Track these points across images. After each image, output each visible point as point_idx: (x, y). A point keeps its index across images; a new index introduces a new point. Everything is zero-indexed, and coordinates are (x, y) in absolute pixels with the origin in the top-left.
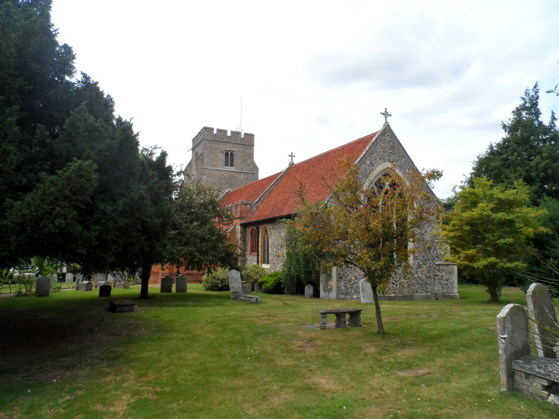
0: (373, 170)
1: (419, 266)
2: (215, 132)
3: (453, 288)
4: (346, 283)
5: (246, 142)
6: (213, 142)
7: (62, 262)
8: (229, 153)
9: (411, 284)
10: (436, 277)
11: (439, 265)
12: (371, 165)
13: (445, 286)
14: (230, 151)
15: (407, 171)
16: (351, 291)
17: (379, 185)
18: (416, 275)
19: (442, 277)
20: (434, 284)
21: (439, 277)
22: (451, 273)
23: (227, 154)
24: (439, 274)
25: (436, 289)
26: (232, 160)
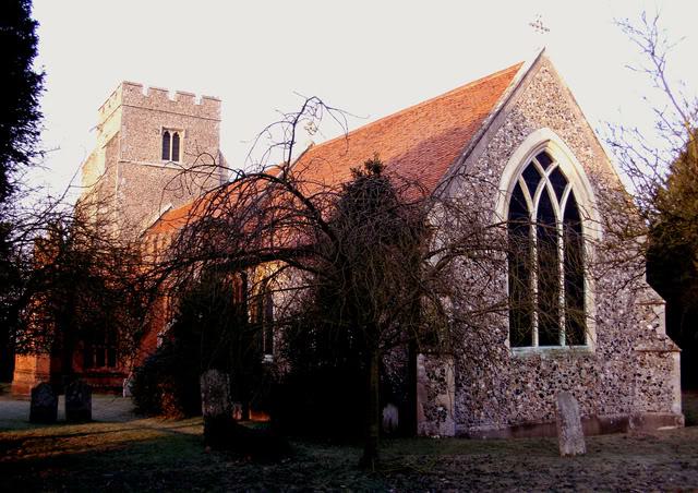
0: (520, 142)
1: (608, 356)
2: (145, 92)
3: (671, 400)
4: (468, 398)
5: (207, 113)
6: (141, 112)
7: (288, 360)
8: (171, 135)
9: (594, 395)
10: (637, 378)
11: (644, 352)
12: (515, 132)
13: (654, 397)
14: (173, 130)
15: (582, 149)
16: (479, 416)
17: (531, 175)
18: (602, 376)
19: (649, 378)
20: (634, 394)
21: (643, 378)
22: (669, 369)
23: (166, 135)
24: (644, 372)
25: (636, 403)
26: (176, 148)
